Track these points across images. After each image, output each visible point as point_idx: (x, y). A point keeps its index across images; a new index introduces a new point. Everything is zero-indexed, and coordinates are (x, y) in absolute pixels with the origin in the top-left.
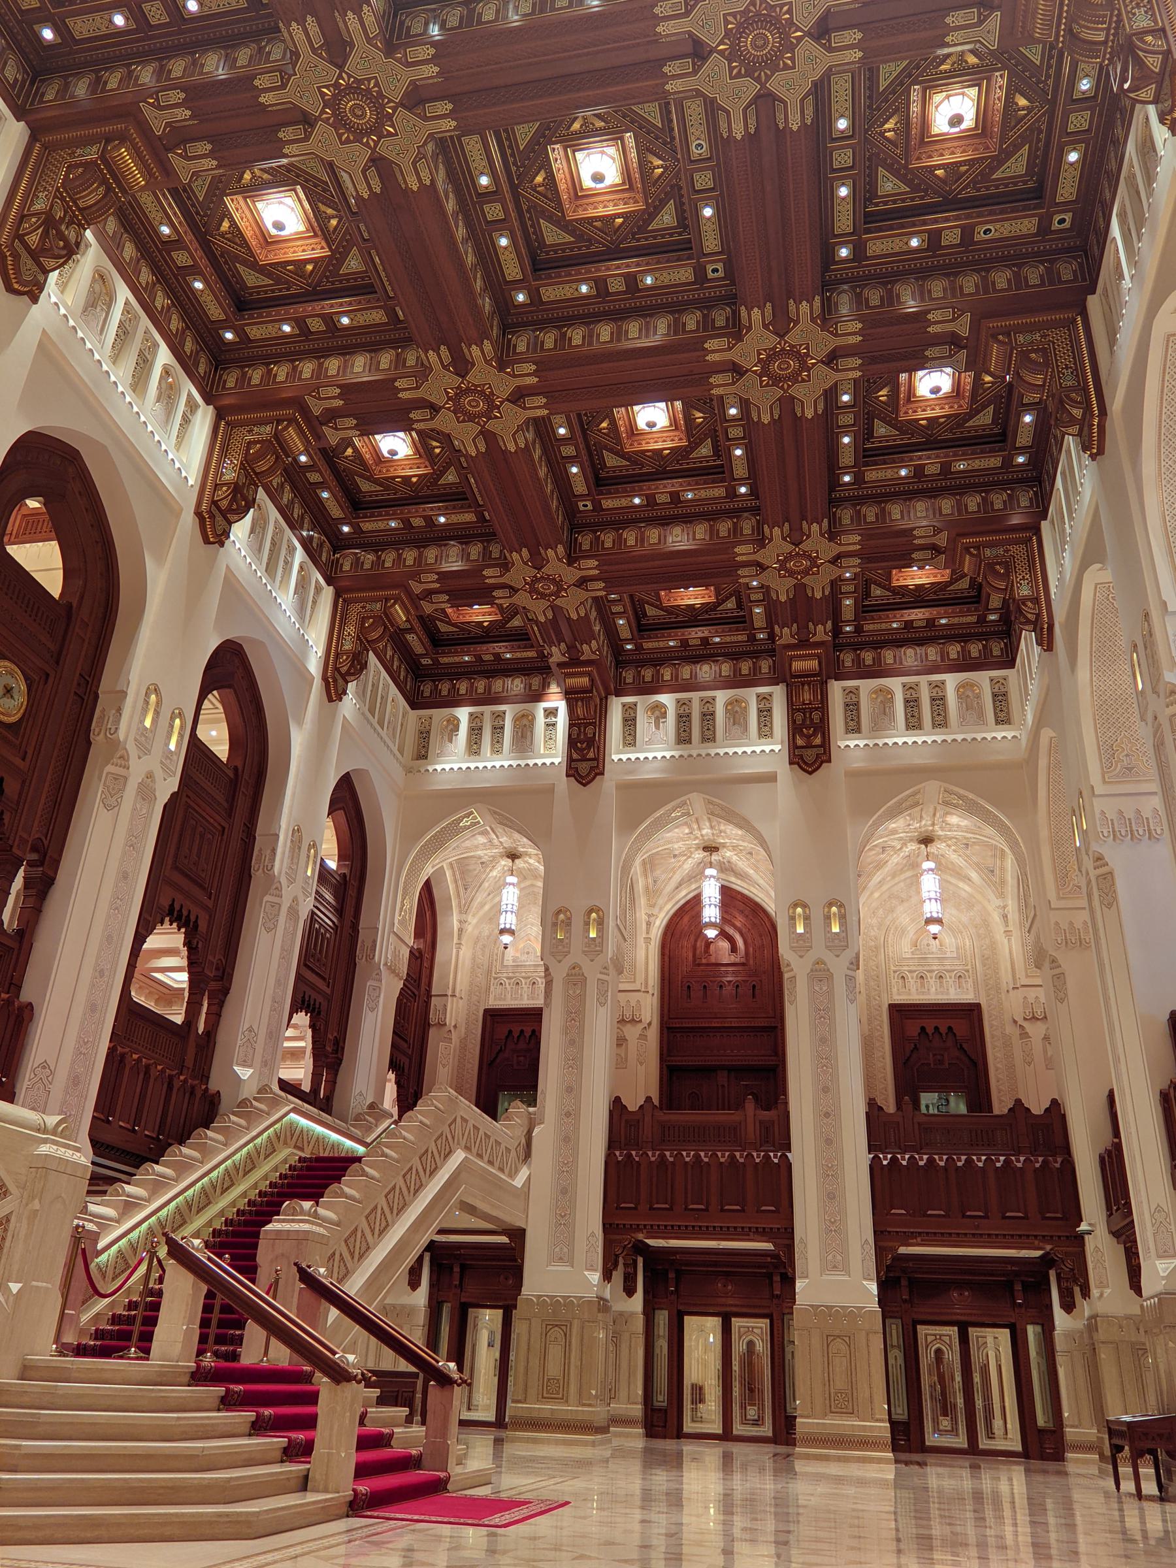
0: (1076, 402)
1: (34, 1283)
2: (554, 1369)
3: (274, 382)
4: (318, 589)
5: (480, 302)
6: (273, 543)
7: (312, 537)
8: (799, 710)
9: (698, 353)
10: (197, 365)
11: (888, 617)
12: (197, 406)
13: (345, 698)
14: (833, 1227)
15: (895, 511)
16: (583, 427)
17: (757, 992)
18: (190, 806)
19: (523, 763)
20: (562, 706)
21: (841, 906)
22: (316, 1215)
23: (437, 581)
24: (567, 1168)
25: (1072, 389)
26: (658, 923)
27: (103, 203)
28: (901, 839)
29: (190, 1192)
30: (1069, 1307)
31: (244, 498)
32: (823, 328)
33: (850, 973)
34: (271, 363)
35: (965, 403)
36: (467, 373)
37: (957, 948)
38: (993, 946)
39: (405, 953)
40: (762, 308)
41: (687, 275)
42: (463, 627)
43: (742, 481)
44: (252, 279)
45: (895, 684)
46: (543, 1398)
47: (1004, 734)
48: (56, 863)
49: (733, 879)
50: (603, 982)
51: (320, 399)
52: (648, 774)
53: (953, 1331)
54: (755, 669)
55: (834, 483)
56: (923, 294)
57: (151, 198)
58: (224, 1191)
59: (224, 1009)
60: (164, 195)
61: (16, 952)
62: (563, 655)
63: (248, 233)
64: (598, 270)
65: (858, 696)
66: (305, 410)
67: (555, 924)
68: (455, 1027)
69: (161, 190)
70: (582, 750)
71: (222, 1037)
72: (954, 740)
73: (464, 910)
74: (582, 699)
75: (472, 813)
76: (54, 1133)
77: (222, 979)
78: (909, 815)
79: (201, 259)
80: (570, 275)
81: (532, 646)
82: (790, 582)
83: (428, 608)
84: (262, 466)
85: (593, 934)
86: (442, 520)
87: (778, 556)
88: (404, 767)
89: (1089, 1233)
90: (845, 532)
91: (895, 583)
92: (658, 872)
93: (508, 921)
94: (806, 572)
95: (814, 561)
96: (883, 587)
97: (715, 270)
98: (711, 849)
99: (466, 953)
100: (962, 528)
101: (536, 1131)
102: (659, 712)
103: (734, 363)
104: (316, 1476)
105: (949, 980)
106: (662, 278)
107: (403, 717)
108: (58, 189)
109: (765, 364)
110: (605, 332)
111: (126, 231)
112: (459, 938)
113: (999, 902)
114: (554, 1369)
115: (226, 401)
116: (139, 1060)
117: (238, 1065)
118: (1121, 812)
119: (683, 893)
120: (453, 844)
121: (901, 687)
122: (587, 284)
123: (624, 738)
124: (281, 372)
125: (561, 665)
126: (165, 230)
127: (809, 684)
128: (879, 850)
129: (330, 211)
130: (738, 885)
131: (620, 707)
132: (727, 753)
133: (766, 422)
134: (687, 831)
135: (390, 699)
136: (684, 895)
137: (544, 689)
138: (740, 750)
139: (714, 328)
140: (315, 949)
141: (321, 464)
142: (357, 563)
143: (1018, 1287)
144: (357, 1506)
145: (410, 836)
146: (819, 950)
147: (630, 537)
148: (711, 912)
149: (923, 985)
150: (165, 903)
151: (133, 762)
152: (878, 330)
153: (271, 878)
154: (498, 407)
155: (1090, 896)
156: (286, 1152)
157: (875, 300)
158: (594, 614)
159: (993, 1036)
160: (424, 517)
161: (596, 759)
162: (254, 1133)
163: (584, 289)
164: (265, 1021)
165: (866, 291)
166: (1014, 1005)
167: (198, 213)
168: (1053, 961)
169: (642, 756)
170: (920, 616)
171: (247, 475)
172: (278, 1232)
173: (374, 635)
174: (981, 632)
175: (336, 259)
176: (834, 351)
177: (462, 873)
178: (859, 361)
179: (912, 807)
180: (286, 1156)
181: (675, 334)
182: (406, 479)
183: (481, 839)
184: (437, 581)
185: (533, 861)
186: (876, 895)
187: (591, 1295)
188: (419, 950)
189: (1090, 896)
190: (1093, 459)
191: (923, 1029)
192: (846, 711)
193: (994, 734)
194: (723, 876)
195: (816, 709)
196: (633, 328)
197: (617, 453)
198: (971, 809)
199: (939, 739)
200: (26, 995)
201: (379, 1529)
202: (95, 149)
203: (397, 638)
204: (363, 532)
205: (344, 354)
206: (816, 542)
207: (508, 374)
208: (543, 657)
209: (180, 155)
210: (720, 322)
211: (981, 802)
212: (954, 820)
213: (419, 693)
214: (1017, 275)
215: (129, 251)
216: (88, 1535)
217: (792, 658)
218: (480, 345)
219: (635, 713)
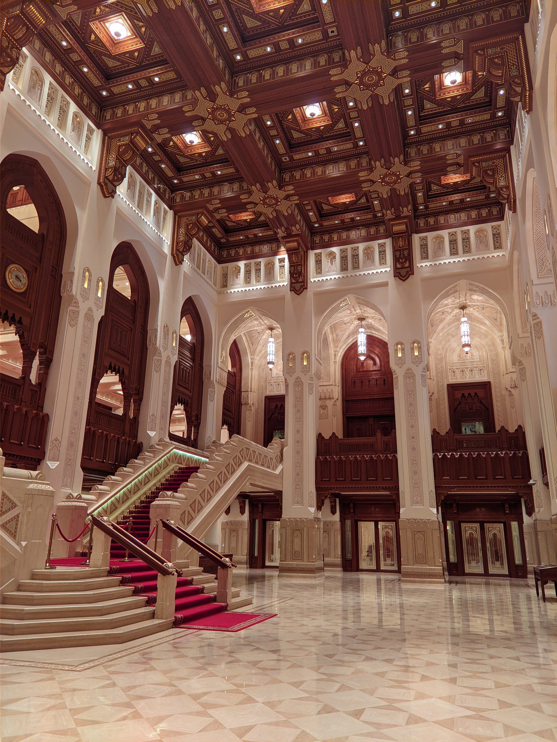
0: (518, 84)
1: (33, 541)
2: (297, 548)
3: (128, 114)
4: (166, 212)
5: (216, 63)
6: (140, 193)
7: (160, 187)
8: (397, 250)
9: (327, 77)
10: (91, 110)
11: (440, 200)
12: (93, 130)
13: (183, 263)
14: (416, 486)
15: (437, 147)
16: (279, 119)
17: (386, 382)
18: (114, 320)
19: (270, 286)
20: (286, 256)
21: (419, 343)
22: (174, 497)
23: (219, 203)
24: (298, 465)
25: (515, 77)
26: (339, 354)
27: (26, 35)
28: (451, 308)
29: (129, 486)
30: (529, 514)
31: (120, 174)
32: (388, 56)
33: (423, 373)
34: (125, 105)
35: (469, 87)
36: (216, 100)
37: (480, 356)
38: (497, 355)
39: (225, 375)
40: (355, 50)
41: (319, 36)
42: (238, 223)
43: (360, 139)
44: (111, 63)
45: (445, 233)
46: (293, 560)
47: (498, 254)
48: (52, 352)
49: (374, 332)
50: (311, 384)
51: (149, 120)
52: (328, 287)
53: (477, 525)
54: (377, 231)
55: (405, 135)
56: (439, 32)
57: (55, 28)
58: (145, 484)
59: (141, 407)
60: (60, 26)
61: (39, 392)
62: (284, 233)
63: (104, 40)
64: (274, 38)
65: (427, 241)
66: (143, 127)
67: (288, 360)
68: (253, 404)
69: (58, 23)
70: (296, 278)
71: (141, 419)
72: (474, 259)
73: (253, 354)
74: (295, 253)
75: (249, 311)
76: (36, 479)
77: (138, 394)
78: (454, 296)
79: (84, 56)
80: (252, 45)
81: (271, 229)
82: (388, 188)
83: (218, 216)
84: (127, 157)
85: (305, 363)
86: (219, 173)
87: (380, 176)
88: (217, 292)
89: (534, 484)
90: (413, 160)
91: (443, 183)
92: (338, 332)
93: (271, 359)
94: (395, 182)
95: (398, 177)
96: (438, 185)
97: (332, 32)
98: (361, 319)
99: (255, 373)
100: (470, 154)
101: (285, 449)
102: (332, 256)
103: (346, 80)
104: (158, 613)
105: (476, 372)
106: (306, 39)
107: (215, 267)
108: (3, 31)
109: (361, 79)
110: (280, 71)
111: (46, 47)
112: (252, 366)
113: (500, 334)
114: (297, 548)
115: (107, 127)
116: (102, 433)
117: (149, 430)
118: (546, 292)
119: (351, 340)
120: (242, 325)
121: (447, 234)
122: (270, 47)
123: (317, 270)
124: (130, 109)
125: (283, 238)
126: (64, 43)
127: (402, 238)
128: (441, 313)
129: (141, 24)
130: (376, 334)
131: (314, 255)
132: (369, 273)
133: (365, 109)
134: (349, 312)
135: (207, 260)
136: (350, 341)
137: (278, 249)
138: (370, 272)
139: (334, 62)
140: (182, 376)
141: (159, 151)
142: (183, 197)
143: (507, 506)
144: (176, 624)
145: (222, 323)
146: (409, 364)
147: (308, 173)
148: (362, 349)
149: (463, 375)
150: (107, 364)
151: (81, 304)
152: (416, 55)
153: (156, 349)
154: (233, 115)
155: (531, 333)
156: (173, 466)
157: (414, 39)
158: (297, 211)
159: (496, 396)
160: (211, 172)
161: (303, 282)
162: (157, 459)
163: (269, 49)
164: (159, 410)
165: (409, 34)
166: (506, 381)
167: (79, 33)
168: (520, 362)
169: (324, 278)
170: (456, 198)
171: (120, 162)
172: (158, 505)
173: (194, 232)
174: (489, 203)
175: (148, 48)
176: (396, 67)
177: (250, 338)
178: (409, 72)
179: (454, 293)
180: (173, 467)
181: (315, 68)
182: (200, 154)
183: (256, 322)
184: (219, 203)
185: (278, 331)
186: (441, 334)
187: (311, 517)
188: (234, 373)
189: (531, 333)
190: (528, 114)
191: (463, 394)
192: (421, 248)
193: (493, 255)
194: (368, 330)
195: (406, 249)
196: (294, 67)
197: (298, 131)
198: (483, 292)
199: (466, 259)
200: (46, 410)
201: (186, 633)
202: (18, 8)
203: (207, 230)
204: (184, 182)
205: (158, 97)
206: (398, 166)
207: (235, 98)
208: (276, 233)
209: (59, 5)
210: (337, 59)
211: (487, 288)
212: (475, 297)
213: (221, 256)
214: (487, 16)
215: (48, 57)
216: (50, 645)
217: (393, 225)
218: (219, 85)
219: (321, 257)
